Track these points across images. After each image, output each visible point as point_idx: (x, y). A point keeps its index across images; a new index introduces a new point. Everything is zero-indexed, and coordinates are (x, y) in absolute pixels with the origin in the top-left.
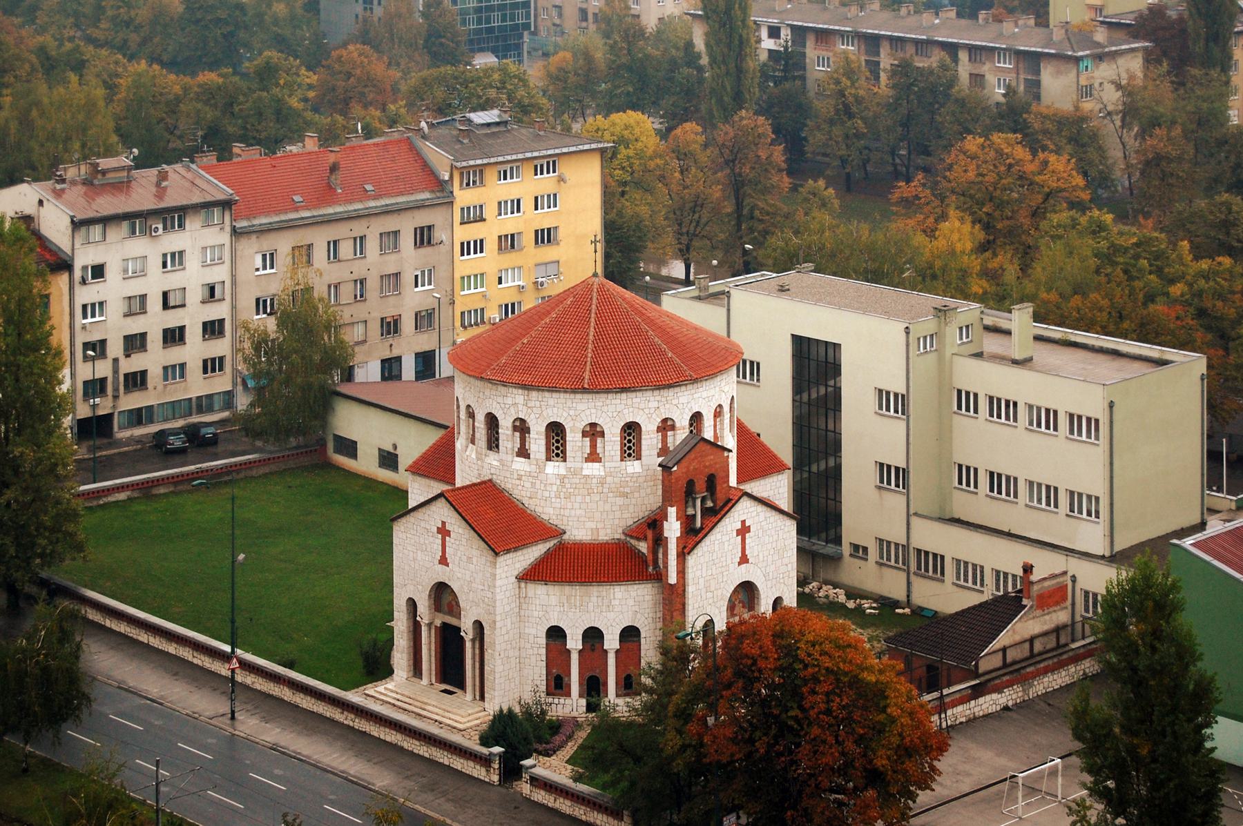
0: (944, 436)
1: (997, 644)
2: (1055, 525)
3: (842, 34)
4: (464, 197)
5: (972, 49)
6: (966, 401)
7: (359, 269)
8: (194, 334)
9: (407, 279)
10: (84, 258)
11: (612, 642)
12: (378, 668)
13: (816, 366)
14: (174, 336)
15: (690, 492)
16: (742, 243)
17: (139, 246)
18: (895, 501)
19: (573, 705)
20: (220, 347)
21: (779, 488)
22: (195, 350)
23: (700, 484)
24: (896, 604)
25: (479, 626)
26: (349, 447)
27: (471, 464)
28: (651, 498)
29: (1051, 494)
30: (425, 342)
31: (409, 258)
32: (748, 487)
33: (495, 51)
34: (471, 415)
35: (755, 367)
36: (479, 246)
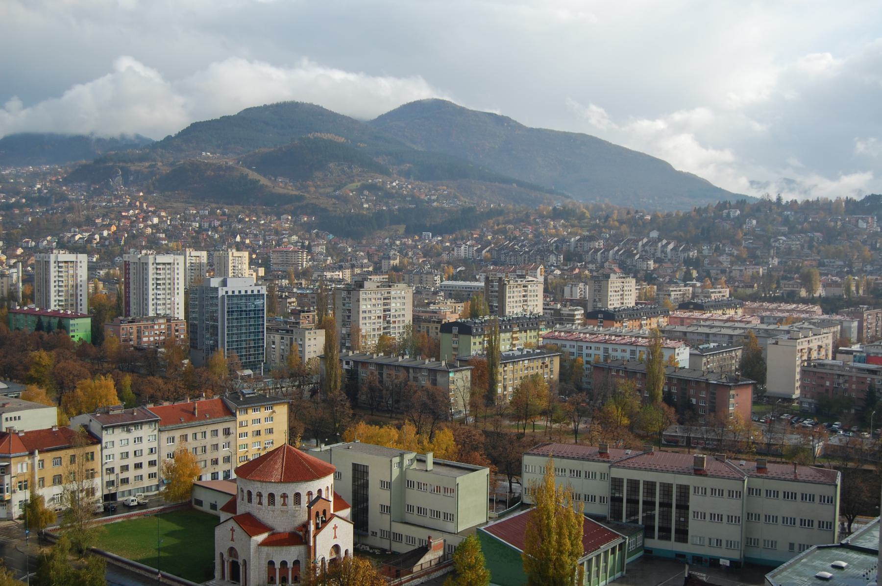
4: (240, 417)
6: (410, 484)
8: (145, 465)
13: (360, 473)
18: (387, 517)
20: (154, 469)
21: (346, 512)
22: (146, 470)
25: (245, 561)
26: (200, 503)
27: (241, 509)
30: (227, 467)
32: (337, 513)
34: (242, 491)
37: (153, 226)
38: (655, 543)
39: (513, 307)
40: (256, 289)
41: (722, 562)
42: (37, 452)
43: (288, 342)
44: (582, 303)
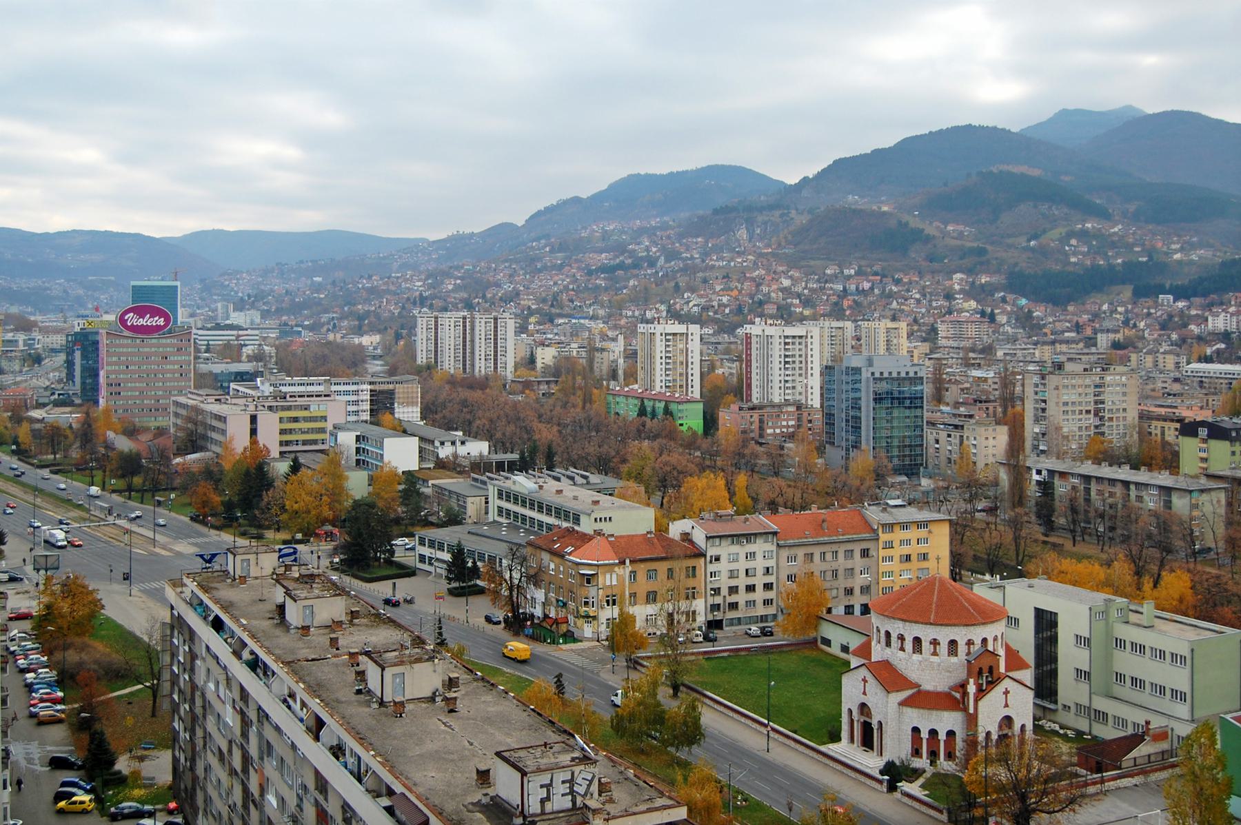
0: (1108, 659)
1: (1131, 755)
2: (1165, 704)
3: (1072, 475)
5: (1137, 484)
6: (1120, 643)
7: (834, 565)
8: (759, 588)
9: (857, 571)
10: (711, 552)
11: (942, 736)
12: (835, 737)
13: (1046, 622)
14: (751, 588)
15: (980, 672)
16: (1007, 566)
17: (735, 549)
18: (1084, 687)
20: (771, 595)
21: (1028, 676)
22: (759, 595)
23: (985, 669)
24: (1084, 733)
25: (880, 723)
26: (827, 642)
28: (961, 675)
29: (1162, 690)
31: (858, 562)
33: (907, 475)
35: (1017, 621)
36: (891, 559)
42: (628, 561)
43: (957, 441)
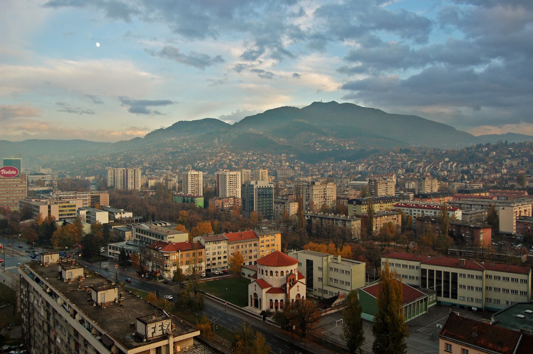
4: (261, 239)
6: (331, 269)
7: (246, 249)
8: (222, 258)
9: (253, 251)
11: (279, 302)
12: (247, 305)
13: (310, 263)
16: (298, 246)
17: (215, 245)
18: (321, 283)
19: (274, 310)
20: (226, 260)
21: (304, 280)
22: (222, 260)
26: (244, 274)
27: (259, 276)
31: (253, 248)
36: (263, 246)
37: (230, 160)
38: (442, 299)
39: (381, 192)
40: (269, 185)
41: (473, 308)
44: (413, 191)
